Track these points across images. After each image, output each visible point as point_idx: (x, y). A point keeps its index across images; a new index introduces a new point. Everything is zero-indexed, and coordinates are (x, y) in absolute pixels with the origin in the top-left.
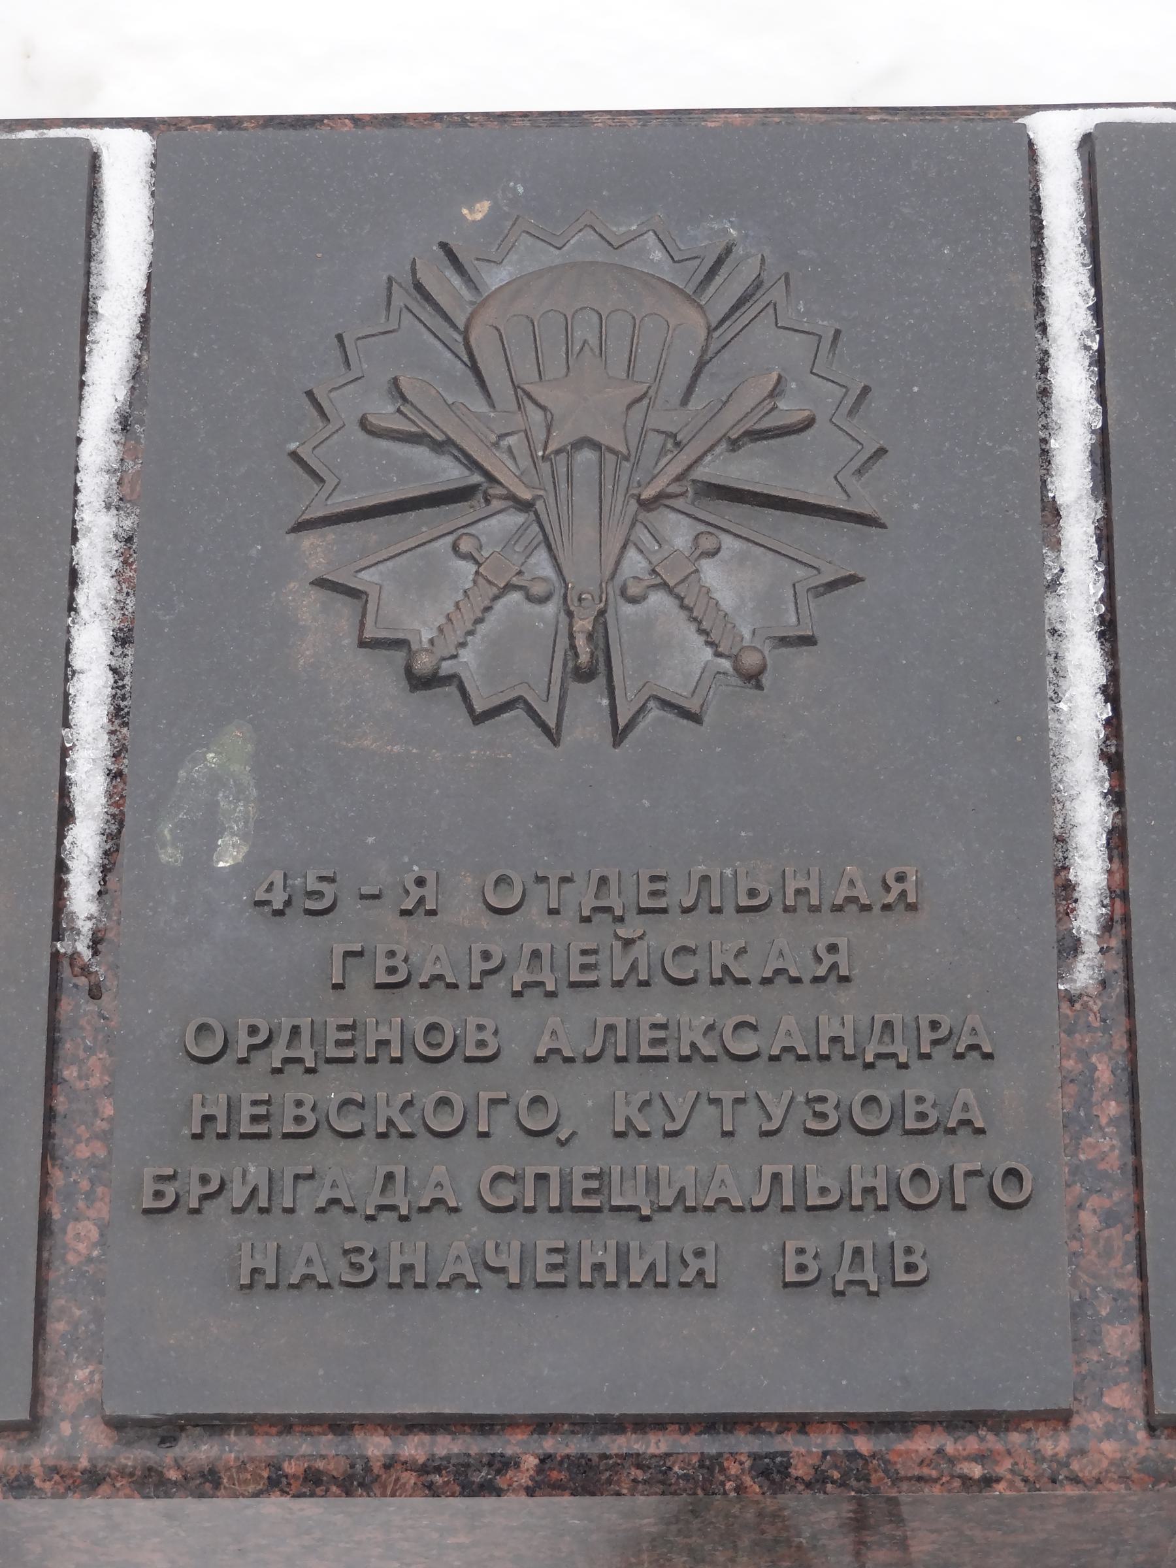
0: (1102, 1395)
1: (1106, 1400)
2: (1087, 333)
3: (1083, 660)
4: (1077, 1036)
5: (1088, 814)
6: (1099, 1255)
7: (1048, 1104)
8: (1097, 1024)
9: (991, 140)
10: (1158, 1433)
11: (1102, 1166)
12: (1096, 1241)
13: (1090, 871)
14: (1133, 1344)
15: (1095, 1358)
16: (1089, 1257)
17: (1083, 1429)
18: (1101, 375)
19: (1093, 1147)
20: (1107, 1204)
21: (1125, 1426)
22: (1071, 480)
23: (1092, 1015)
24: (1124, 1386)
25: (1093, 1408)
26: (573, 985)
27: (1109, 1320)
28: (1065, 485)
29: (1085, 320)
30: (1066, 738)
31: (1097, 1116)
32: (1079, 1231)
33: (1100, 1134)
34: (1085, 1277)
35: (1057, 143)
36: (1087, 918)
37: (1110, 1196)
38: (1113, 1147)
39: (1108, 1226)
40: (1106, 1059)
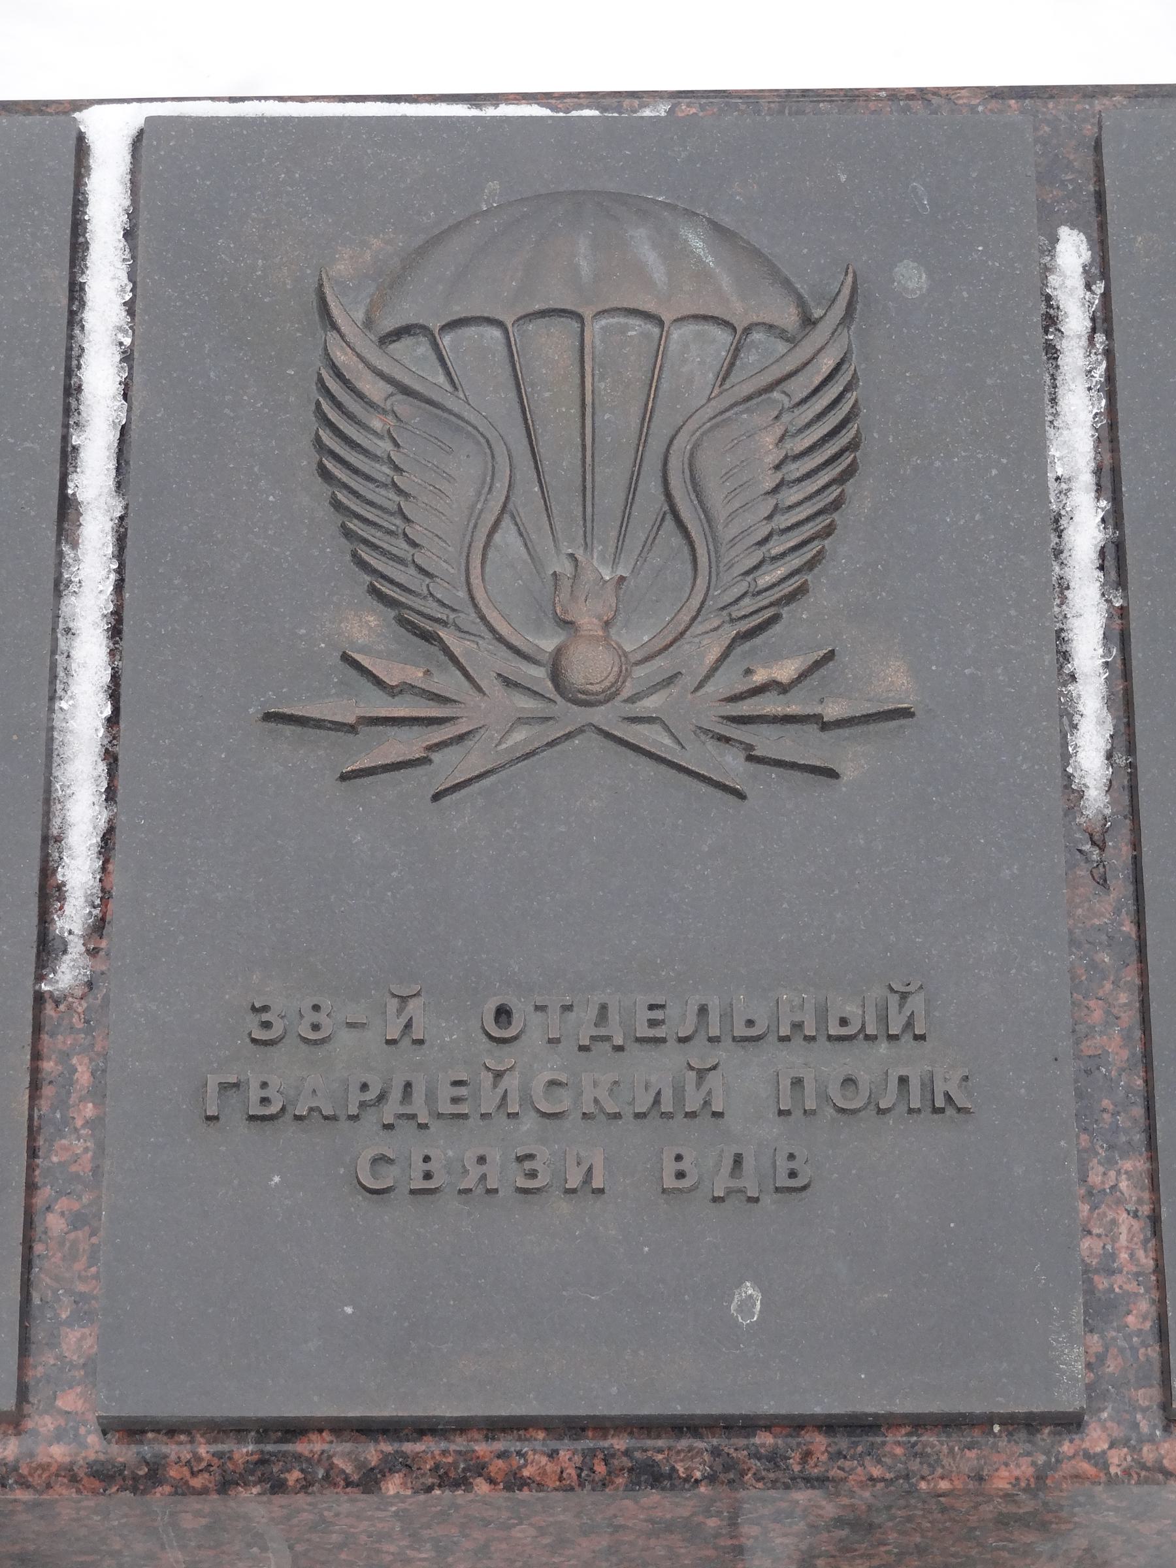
0: (55, 1399)
1: (59, 1403)
2: (120, 329)
3: (89, 658)
4: (59, 1037)
5: (82, 814)
6: (64, 1258)
7: (14, 1105)
8: (80, 1026)
9: (48, 133)
10: (109, 1436)
11: (74, 1168)
12: (62, 1243)
13: (79, 871)
14: (91, 1347)
15: (52, 1362)
16: (53, 1260)
17: (35, 1433)
18: (69, 372)
19: (66, 1149)
20: (76, 1206)
21: (76, 1429)
22: (94, 480)
23: (76, 1016)
24: (79, 1390)
25: (46, 1412)
26: (640, 1040)
27: (69, 1323)
28: (85, 482)
29: (119, 316)
30: (69, 737)
31: (74, 1118)
32: (46, 1233)
33: (74, 1136)
34: (48, 1280)
35: (109, 138)
36: (73, 918)
37: (80, 1197)
38: (86, 1149)
39: (76, 1229)
40: (86, 1060)
